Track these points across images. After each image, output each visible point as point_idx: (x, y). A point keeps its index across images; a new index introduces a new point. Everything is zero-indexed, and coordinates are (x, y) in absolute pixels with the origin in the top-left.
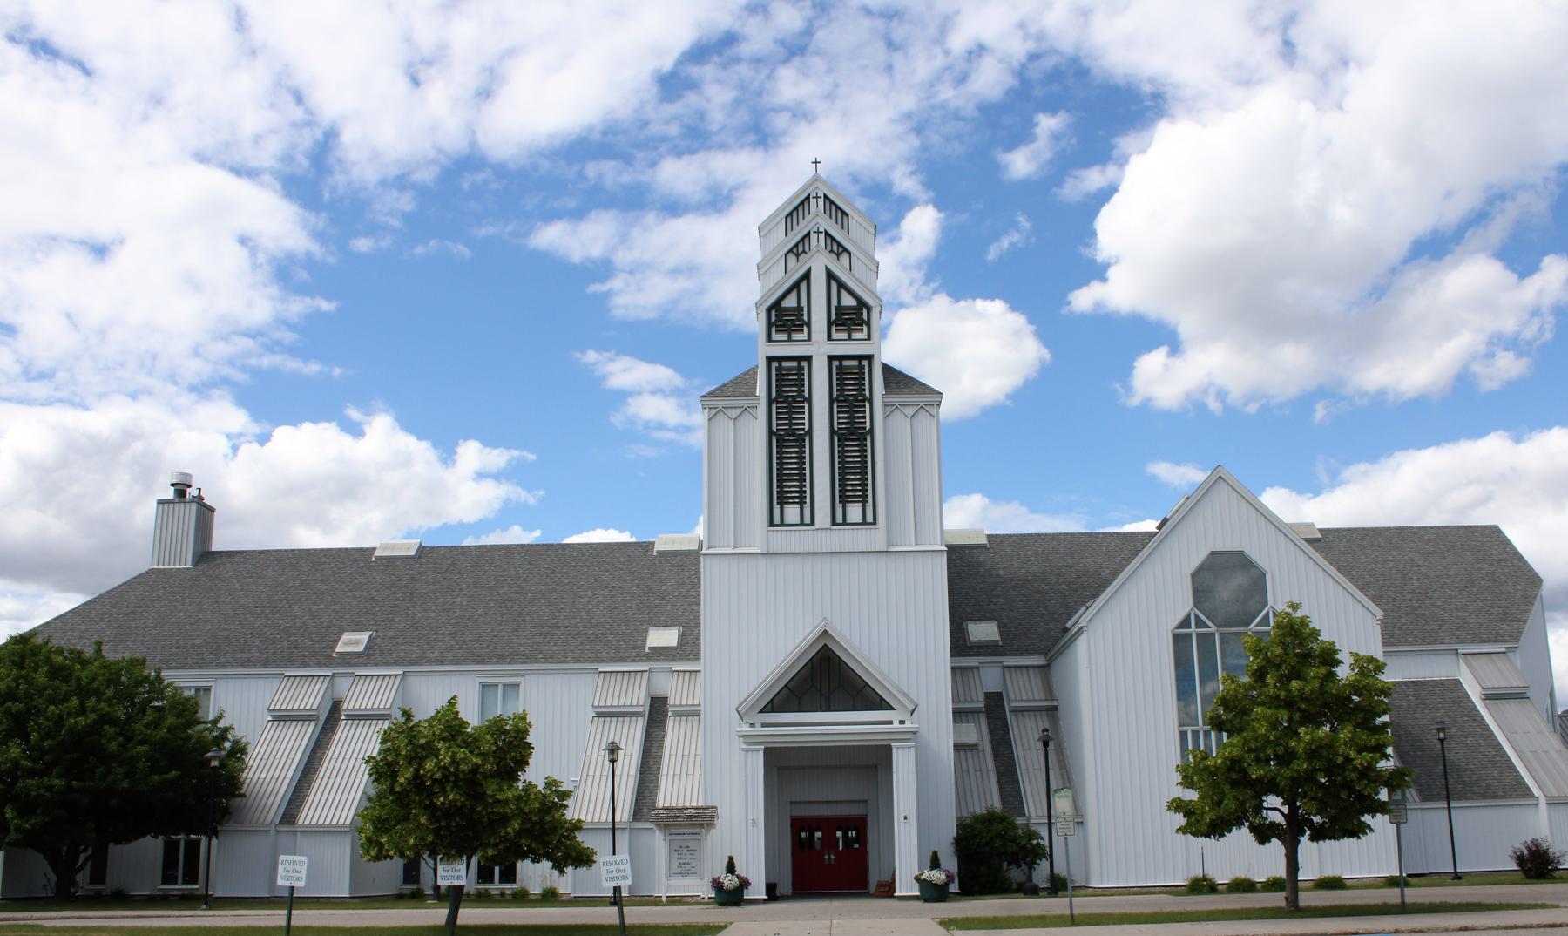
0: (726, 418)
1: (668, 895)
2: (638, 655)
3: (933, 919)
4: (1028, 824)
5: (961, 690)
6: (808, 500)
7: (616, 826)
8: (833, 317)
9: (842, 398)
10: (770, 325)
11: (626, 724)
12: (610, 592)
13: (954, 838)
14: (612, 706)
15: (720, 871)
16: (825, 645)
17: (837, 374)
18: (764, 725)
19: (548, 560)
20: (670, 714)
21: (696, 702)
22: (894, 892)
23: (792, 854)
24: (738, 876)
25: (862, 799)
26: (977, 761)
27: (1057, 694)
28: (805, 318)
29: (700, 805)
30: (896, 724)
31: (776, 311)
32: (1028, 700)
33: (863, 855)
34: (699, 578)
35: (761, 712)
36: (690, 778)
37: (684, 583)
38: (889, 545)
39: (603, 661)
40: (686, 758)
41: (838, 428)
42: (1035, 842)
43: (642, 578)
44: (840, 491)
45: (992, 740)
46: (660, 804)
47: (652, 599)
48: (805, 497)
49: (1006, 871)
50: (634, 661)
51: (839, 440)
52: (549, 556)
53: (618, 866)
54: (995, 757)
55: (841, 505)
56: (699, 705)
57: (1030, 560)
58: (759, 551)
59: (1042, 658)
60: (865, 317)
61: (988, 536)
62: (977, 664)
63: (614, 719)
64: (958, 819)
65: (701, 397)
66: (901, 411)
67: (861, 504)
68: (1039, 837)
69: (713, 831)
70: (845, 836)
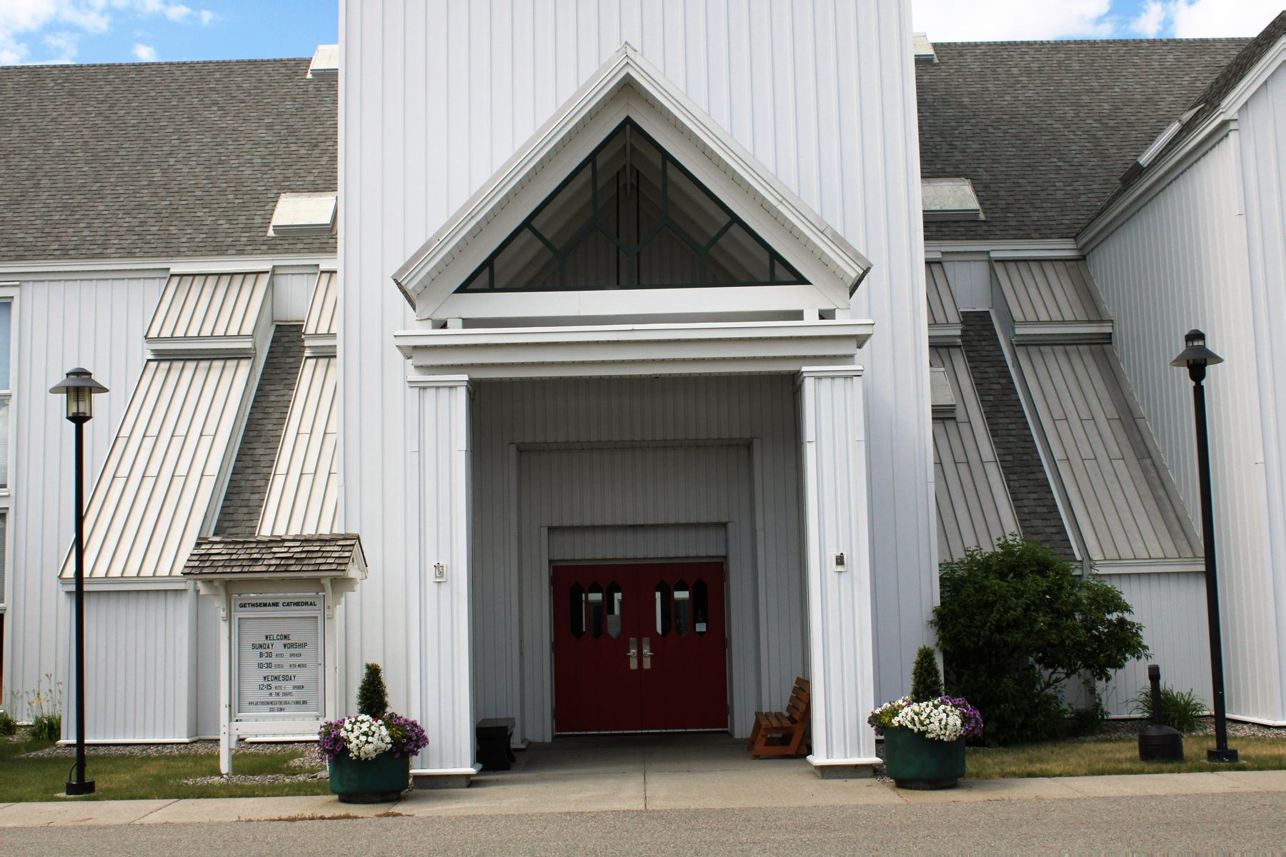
2: (251, 242)
7: (86, 588)
12: (217, 136)
13: (936, 611)
16: (628, 121)
18: (468, 323)
19: (108, 88)
24: (393, 723)
27: (1109, 310)
33: (718, 644)
35: (464, 289)
39: (179, 254)
42: (1114, 617)
43: (279, 114)
46: (265, 531)
47: (293, 147)
50: (241, 252)
52: (109, 83)
57: (1018, 82)
69: (353, 597)
70: (667, 598)
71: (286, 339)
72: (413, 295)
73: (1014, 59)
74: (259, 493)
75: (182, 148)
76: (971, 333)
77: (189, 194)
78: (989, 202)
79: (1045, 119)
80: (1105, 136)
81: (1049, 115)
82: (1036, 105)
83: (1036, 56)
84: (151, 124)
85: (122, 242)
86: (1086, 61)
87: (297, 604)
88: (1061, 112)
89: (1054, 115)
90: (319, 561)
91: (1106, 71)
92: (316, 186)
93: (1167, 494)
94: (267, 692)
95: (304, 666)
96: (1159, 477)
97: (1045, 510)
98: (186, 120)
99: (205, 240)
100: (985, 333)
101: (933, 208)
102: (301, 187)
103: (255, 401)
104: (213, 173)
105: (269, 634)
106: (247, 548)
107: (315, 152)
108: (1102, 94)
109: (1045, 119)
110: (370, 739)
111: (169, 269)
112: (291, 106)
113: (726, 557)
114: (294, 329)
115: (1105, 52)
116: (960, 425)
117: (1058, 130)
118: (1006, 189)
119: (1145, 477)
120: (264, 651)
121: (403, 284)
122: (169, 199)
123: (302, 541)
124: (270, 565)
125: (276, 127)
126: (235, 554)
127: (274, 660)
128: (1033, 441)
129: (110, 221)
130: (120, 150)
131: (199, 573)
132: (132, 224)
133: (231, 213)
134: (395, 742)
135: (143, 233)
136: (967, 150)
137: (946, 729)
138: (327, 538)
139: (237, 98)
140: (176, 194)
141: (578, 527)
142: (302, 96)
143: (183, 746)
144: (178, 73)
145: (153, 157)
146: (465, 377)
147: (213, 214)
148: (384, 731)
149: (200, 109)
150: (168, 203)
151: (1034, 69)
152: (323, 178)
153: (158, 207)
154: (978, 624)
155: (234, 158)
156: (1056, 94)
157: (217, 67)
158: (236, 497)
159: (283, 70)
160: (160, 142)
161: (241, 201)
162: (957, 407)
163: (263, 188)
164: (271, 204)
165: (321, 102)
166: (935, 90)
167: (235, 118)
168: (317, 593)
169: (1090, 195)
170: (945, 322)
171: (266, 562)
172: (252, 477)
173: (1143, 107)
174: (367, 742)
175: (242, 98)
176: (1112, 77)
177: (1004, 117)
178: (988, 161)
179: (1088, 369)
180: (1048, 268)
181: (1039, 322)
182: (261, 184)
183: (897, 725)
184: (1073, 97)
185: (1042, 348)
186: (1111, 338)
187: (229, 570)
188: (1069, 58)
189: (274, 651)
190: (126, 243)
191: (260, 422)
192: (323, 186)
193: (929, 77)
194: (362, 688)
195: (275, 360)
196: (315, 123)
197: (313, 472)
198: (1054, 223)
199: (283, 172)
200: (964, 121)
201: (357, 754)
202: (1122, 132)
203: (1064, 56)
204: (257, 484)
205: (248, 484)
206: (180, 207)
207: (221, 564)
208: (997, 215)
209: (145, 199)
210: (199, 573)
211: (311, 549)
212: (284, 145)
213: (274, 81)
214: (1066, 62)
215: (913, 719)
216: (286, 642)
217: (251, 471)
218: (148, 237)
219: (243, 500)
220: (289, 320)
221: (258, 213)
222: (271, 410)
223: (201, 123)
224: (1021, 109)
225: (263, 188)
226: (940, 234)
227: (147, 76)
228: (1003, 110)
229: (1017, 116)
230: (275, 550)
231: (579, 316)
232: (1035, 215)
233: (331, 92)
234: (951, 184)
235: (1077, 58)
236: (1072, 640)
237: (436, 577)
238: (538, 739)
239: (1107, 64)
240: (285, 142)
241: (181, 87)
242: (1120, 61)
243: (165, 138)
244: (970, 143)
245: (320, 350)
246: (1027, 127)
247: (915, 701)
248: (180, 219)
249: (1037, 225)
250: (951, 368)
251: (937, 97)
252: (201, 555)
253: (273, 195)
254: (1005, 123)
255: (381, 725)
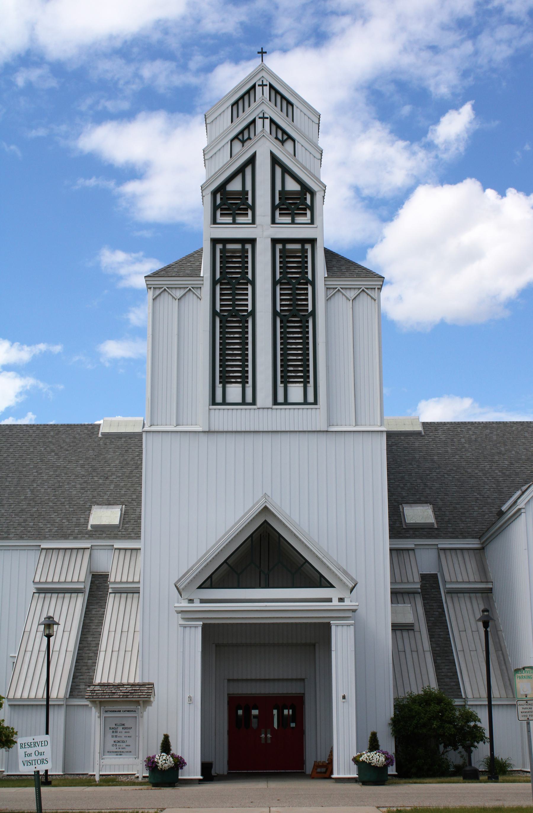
0: (170, 297)
1: (101, 773)
2: (80, 532)
3: (378, 807)
4: (464, 705)
5: (397, 571)
6: (250, 380)
7: (50, 703)
8: (277, 201)
9: (285, 281)
10: (215, 208)
11: (66, 601)
12: (55, 471)
13: (392, 719)
14: (52, 582)
15: (155, 750)
16: (265, 521)
17: (280, 257)
18: (202, 601)
20: (110, 591)
21: (136, 580)
22: (332, 773)
23: (229, 732)
24: (173, 756)
25: (299, 677)
26: (413, 642)
27: (491, 576)
28: (250, 276)
29: (137, 681)
30: (335, 602)
31: (221, 195)
32: (463, 582)
33: (300, 731)
34: (141, 459)
35: (200, 587)
36: (128, 654)
37: (128, 464)
38: (329, 425)
40: (125, 634)
41: (281, 310)
42: (472, 724)
43: (87, 459)
44: (282, 371)
45: (428, 621)
46: (97, 680)
48: (247, 377)
49: (443, 753)
50: (75, 538)
51: (281, 322)
53: (36, 749)
54: (430, 638)
55: (282, 385)
56: (139, 582)
58: (200, 429)
59: (477, 541)
60: (308, 202)
61: (424, 424)
62: (413, 546)
63: (55, 596)
64: (396, 700)
65: (145, 277)
66: (343, 294)
67: (302, 385)
68: (476, 719)
69: (149, 709)
70: (280, 714)
71: (97, 582)
72: (181, 590)
73: (463, 433)
74: (92, 659)
75: (39, 477)
76: (427, 585)
77: (46, 505)
78: (440, 518)
79: (474, 470)
80: (503, 481)
81: (477, 468)
82: (471, 462)
83: (475, 431)
84: (21, 463)
85: (16, 531)
86: (500, 435)
87: (128, 711)
88: (483, 466)
89: (479, 468)
90: (139, 694)
91: (510, 441)
92: (109, 502)
93: (506, 668)
94: (115, 747)
95: (130, 737)
96: (504, 660)
97: (452, 674)
98: (39, 460)
99: (57, 531)
100: (434, 585)
101: (412, 522)
102: (102, 502)
103: (85, 614)
104: (57, 493)
105: (116, 723)
106: (109, 688)
107: (107, 482)
108: (506, 455)
109: (474, 470)
110: (166, 762)
111: (40, 546)
112: (92, 454)
113: (304, 694)
114: (101, 577)
115: (511, 429)
116: (415, 633)
117: (480, 476)
118: (450, 511)
119: (498, 659)
120: (114, 730)
121: (178, 587)
122: (36, 507)
123: (131, 685)
124: (120, 695)
125: (85, 467)
126: (105, 690)
127: (118, 734)
128: (450, 641)
129: (8, 519)
130: (8, 478)
131: (92, 698)
132: (20, 521)
133: (68, 516)
134: (175, 764)
135: (26, 526)
136: (433, 488)
137: (378, 762)
138: (142, 684)
139: (64, 448)
140: (39, 505)
141: (240, 680)
142: (97, 448)
143: (60, 776)
144: (31, 431)
145: (25, 482)
146: (201, 623)
147: (59, 516)
148: (171, 759)
149: (45, 454)
150: (36, 509)
151: (473, 439)
152: (112, 497)
153: (31, 512)
154: (409, 725)
155: (66, 484)
156: (482, 455)
157: (51, 428)
158: (81, 661)
159: (86, 431)
160: (27, 473)
161: (73, 509)
162: (415, 624)
163: (83, 502)
164: (87, 511)
165: (108, 452)
166: (420, 452)
167: (64, 460)
168: (137, 707)
169: (490, 515)
170: (413, 581)
171: (118, 694)
172: (88, 652)
173: (525, 463)
174: (165, 763)
175: (66, 448)
176: (512, 445)
177: (454, 468)
178: (442, 494)
179: (479, 605)
180: (466, 553)
181: (457, 582)
182: (82, 500)
183: (361, 760)
184: (490, 457)
185: (459, 594)
186: (492, 590)
187: (104, 697)
188: (491, 433)
189: (119, 730)
190: (18, 532)
191: (89, 624)
192: (113, 502)
193: (418, 443)
194: (162, 744)
195: (93, 593)
196: (105, 464)
197: (118, 650)
198: (470, 530)
199: (92, 493)
200: (433, 470)
201: (161, 767)
202: (512, 478)
203: (489, 431)
204: (90, 655)
205: (86, 655)
206: (43, 512)
207: (100, 694)
208: (443, 525)
209: (24, 507)
210: (92, 698)
211: (135, 689)
212: (91, 477)
213: (82, 438)
214: (490, 435)
215: (367, 758)
216: (123, 727)
217: (87, 648)
218: (29, 529)
219: (84, 663)
220: (98, 572)
221: (82, 516)
222: (93, 619)
223: (47, 463)
224: (463, 464)
225: (83, 502)
226: (414, 535)
227: (15, 433)
228: (454, 464)
229: (461, 468)
230: (121, 689)
231: (245, 599)
232: (462, 525)
233: (112, 446)
234: (422, 508)
235: (496, 433)
236: (448, 733)
237: (189, 701)
238: (221, 773)
239: (511, 437)
240: (91, 475)
241: (34, 440)
242: (518, 435)
243: (30, 471)
244: (434, 483)
245: (116, 589)
246: (465, 474)
247: (369, 752)
248: (44, 519)
249: (462, 531)
250: (414, 605)
251: (421, 456)
252: (91, 690)
253: (88, 507)
254: (454, 472)
255: (170, 757)
